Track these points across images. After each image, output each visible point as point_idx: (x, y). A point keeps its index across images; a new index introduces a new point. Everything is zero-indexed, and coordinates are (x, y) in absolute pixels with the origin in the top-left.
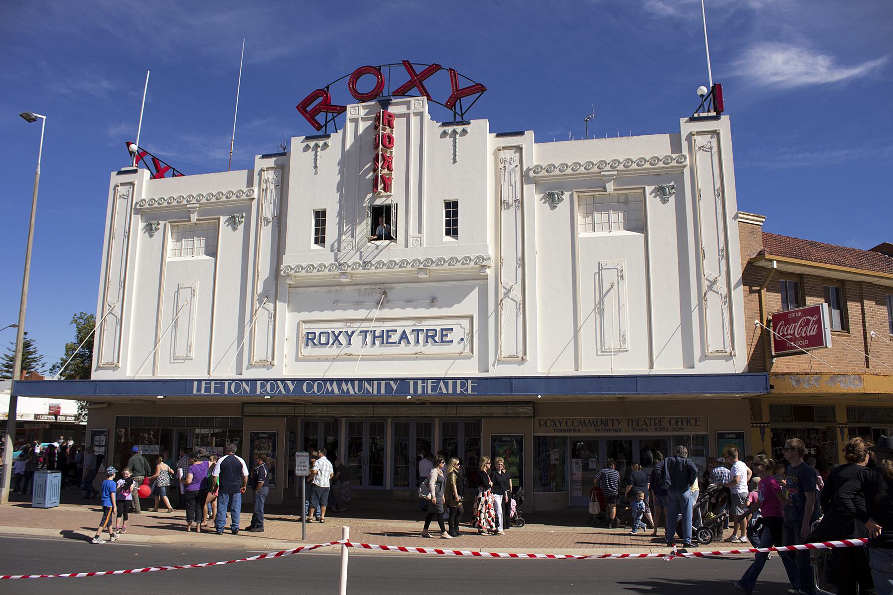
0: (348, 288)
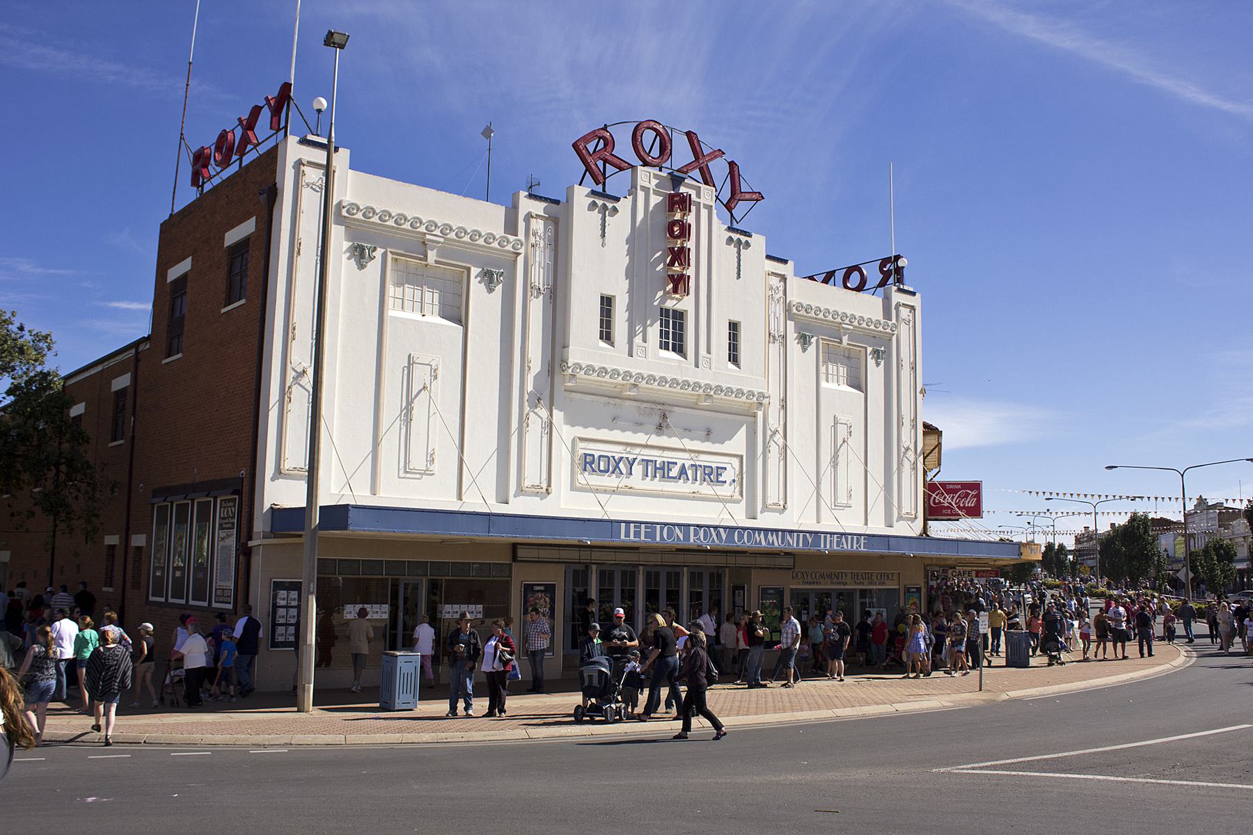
0: (628, 402)
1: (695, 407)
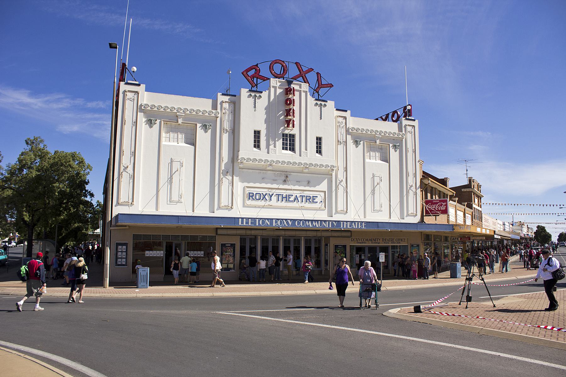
1: (302, 172)
